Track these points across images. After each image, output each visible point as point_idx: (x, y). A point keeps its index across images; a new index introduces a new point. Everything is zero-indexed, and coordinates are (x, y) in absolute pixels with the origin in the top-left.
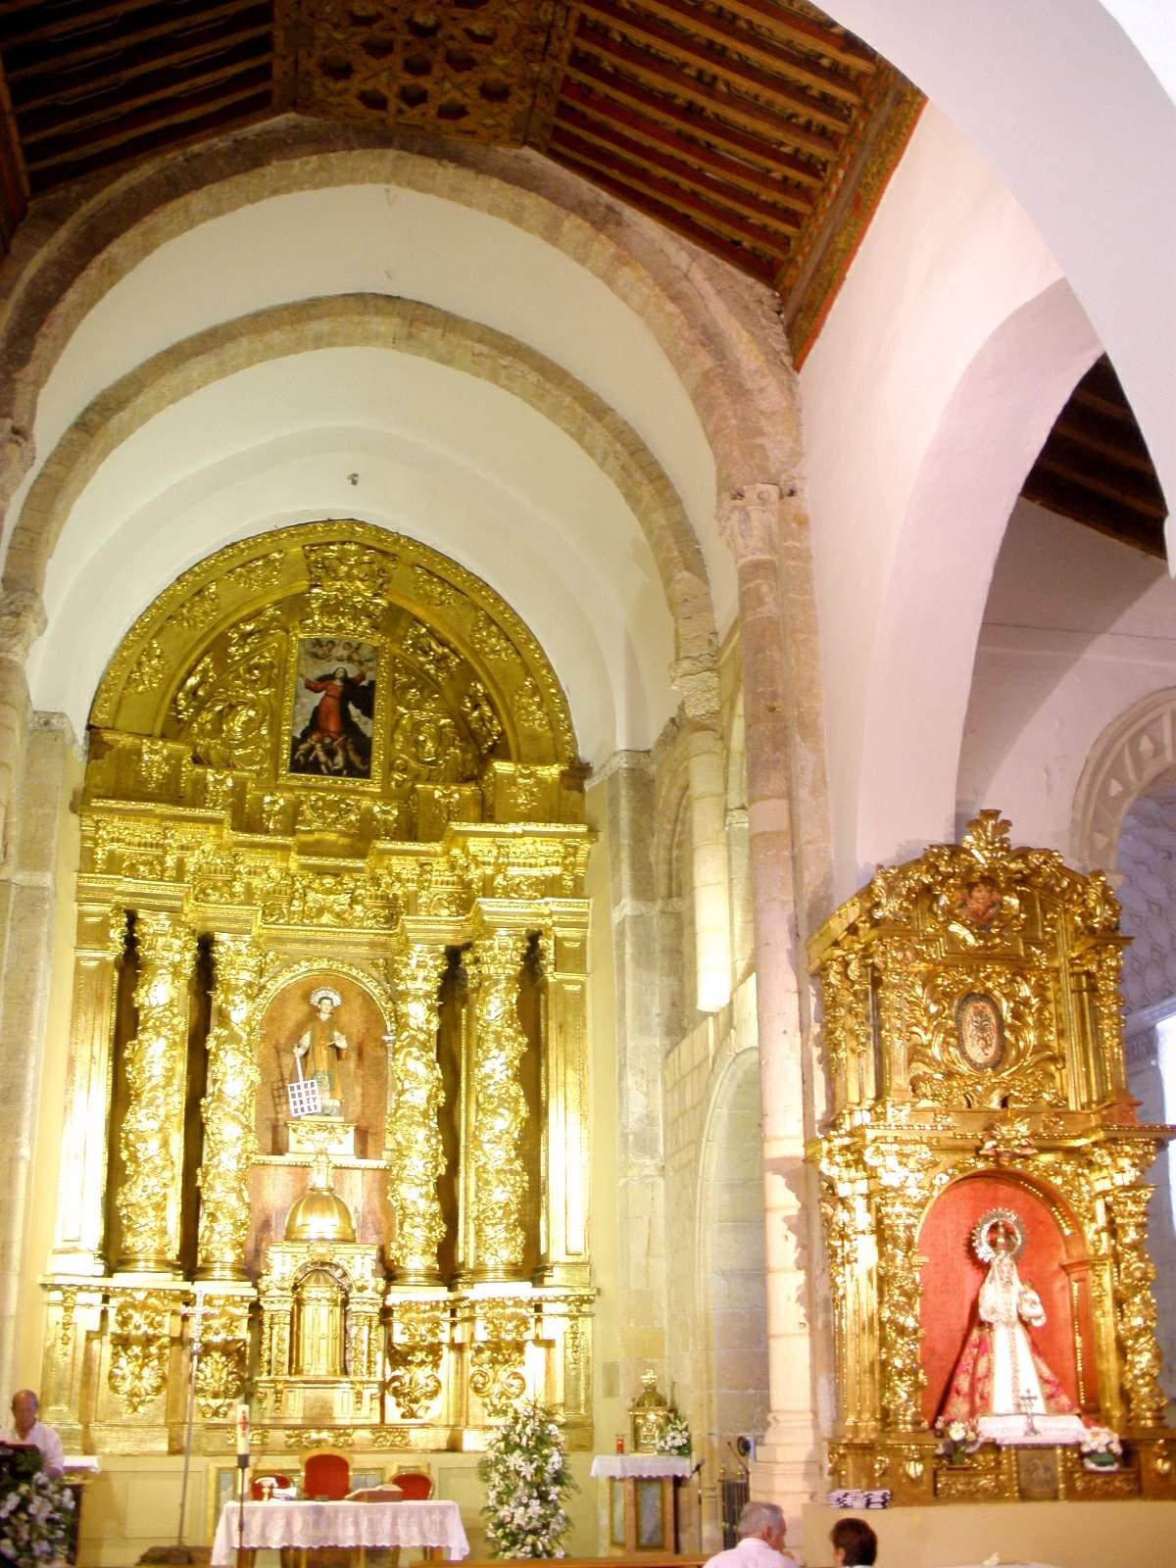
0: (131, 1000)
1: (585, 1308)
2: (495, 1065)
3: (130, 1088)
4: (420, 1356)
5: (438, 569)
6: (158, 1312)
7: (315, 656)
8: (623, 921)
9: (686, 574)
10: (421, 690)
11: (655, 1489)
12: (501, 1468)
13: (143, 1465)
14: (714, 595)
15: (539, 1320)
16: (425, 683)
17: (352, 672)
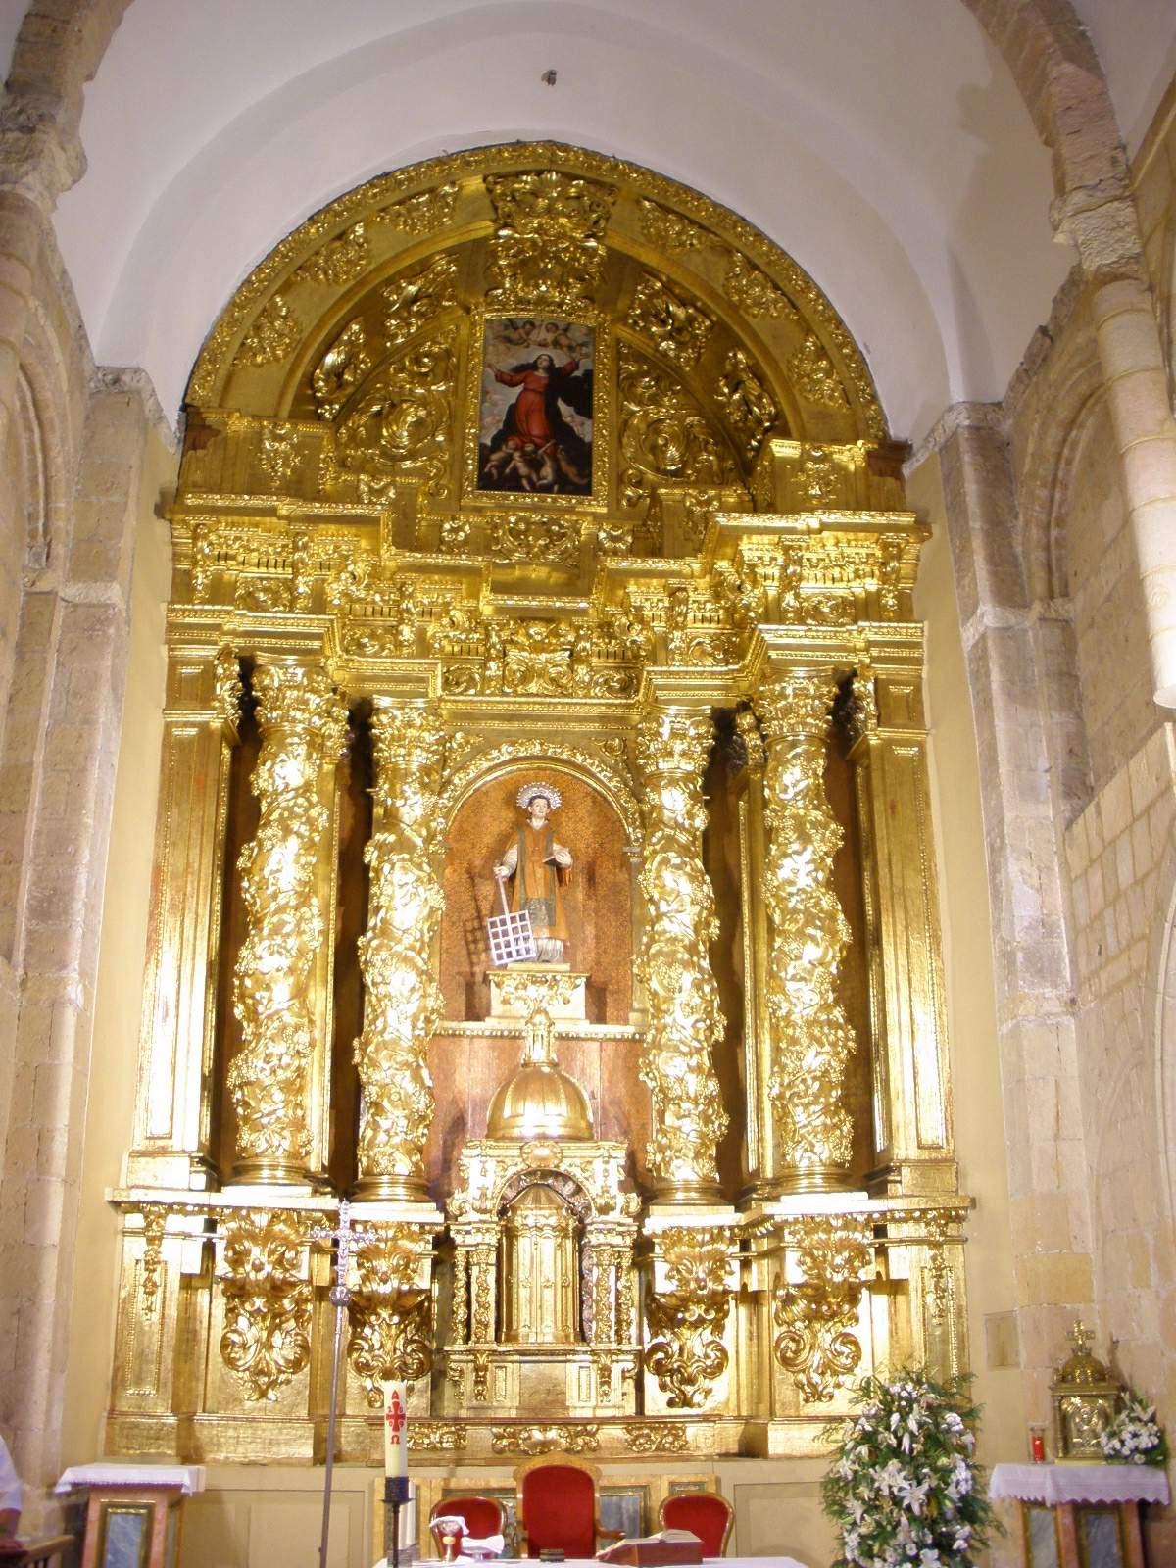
0: (249, 785)
1: (952, 1229)
2: (799, 869)
3: (247, 913)
4: (696, 1311)
5: (672, 200)
6: (291, 1245)
7: (508, 340)
8: (983, 637)
9: (1068, 68)
10: (657, 380)
11: (1108, 1524)
12: (867, 1494)
13: (271, 1479)
14: (1114, 94)
15: (882, 1252)
16: (665, 373)
17: (560, 359)
